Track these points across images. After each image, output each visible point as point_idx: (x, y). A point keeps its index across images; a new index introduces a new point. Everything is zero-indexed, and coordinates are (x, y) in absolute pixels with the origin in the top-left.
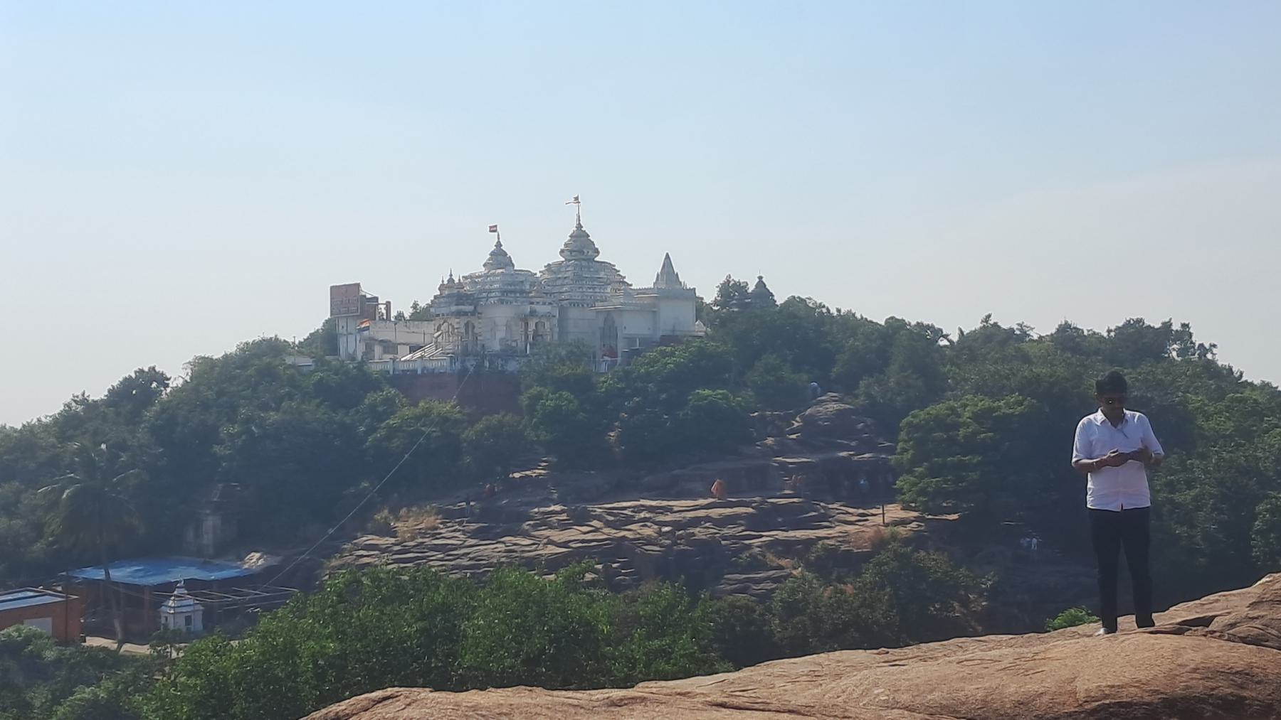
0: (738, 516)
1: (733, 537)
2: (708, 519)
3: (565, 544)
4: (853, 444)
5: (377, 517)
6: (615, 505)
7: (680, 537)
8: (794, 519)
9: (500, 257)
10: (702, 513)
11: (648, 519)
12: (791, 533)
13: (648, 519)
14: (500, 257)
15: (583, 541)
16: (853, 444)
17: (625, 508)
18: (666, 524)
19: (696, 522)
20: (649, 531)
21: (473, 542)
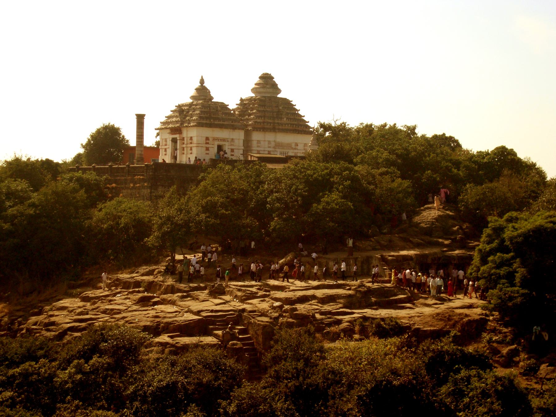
0: (338, 297)
1: (330, 313)
2: (314, 297)
3: (198, 313)
4: (446, 242)
5: (32, 212)
6: (247, 283)
7: (286, 311)
8: (385, 300)
9: (203, 92)
10: (310, 293)
11: (258, 300)
12: (202, 339)
13: (258, 300)
14: (203, 92)
15: (212, 311)
16: (446, 242)
17: (252, 286)
18: (277, 300)
19: (304, 300)
20: (265, 306)
21: (135, 307)
